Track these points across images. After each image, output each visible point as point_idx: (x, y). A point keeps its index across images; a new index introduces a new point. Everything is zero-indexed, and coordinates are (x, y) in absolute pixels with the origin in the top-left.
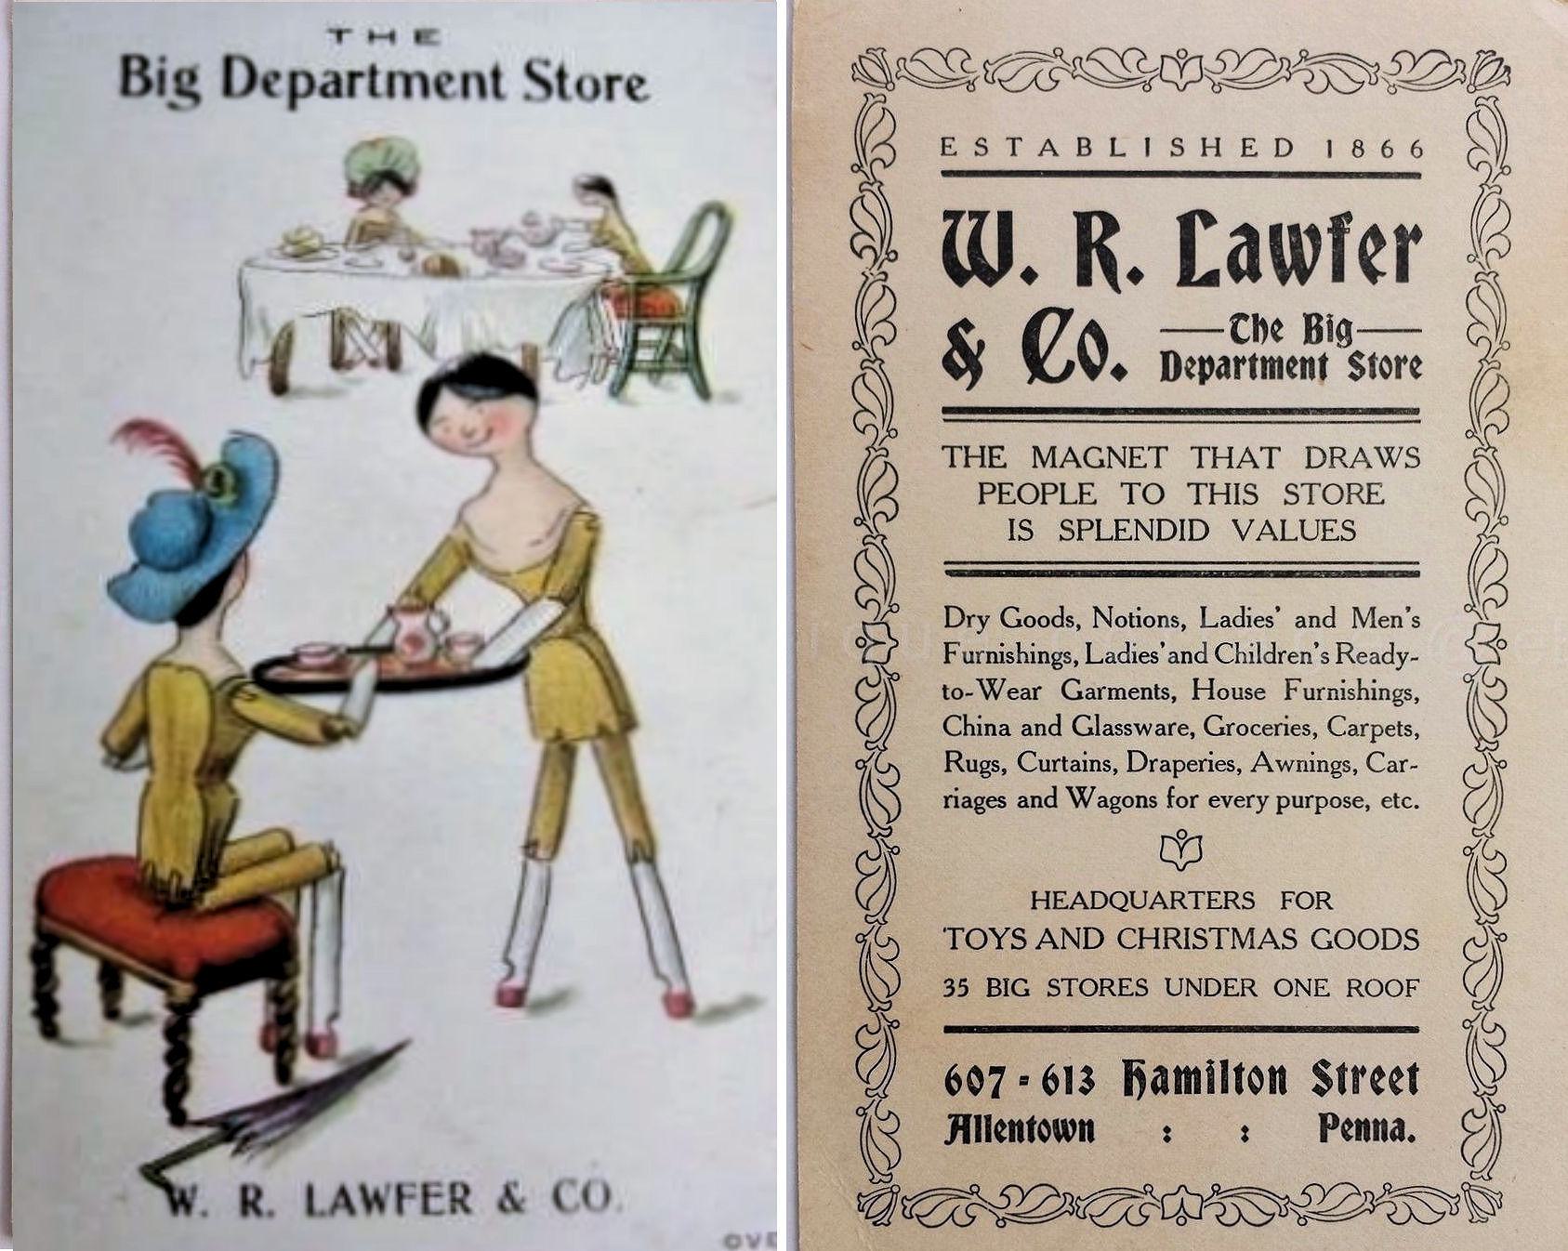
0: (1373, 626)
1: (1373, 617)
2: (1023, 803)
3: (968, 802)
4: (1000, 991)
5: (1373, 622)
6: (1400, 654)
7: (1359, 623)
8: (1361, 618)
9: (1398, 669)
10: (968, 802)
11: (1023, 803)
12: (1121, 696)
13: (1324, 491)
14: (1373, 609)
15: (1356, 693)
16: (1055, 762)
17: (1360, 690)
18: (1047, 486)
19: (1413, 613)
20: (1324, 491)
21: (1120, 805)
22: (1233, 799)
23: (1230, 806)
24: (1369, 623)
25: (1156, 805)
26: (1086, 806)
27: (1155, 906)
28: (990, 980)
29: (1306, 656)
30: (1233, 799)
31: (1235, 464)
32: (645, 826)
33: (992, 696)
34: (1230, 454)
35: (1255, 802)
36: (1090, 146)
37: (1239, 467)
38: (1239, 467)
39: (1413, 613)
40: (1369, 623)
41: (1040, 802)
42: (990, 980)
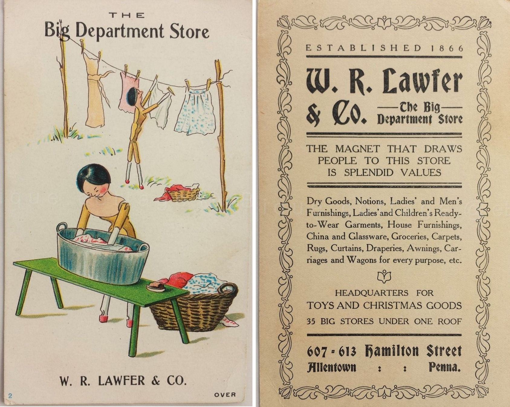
0: (447, 204)
1: (447, 201)
2: (333, 261)
5: (447, 202)
6: (455, 213)
9: (455, 218)
11: (333, 261)
12: (364, 226)
13: (431, 160)
14: (446, 198)
19: (460, 199)
20: (431, 160)
21: (364, 262)
22: (401, 260)
24: (445, 203)
25: (376, 262)
26: (353, 262)
30: (401, 260)
31: (402, 151)
34: (400, 148)
35: (408, 261)
37: (403, 152)
38: (403, 152)
39: (460, 199)
41: (338, 261)
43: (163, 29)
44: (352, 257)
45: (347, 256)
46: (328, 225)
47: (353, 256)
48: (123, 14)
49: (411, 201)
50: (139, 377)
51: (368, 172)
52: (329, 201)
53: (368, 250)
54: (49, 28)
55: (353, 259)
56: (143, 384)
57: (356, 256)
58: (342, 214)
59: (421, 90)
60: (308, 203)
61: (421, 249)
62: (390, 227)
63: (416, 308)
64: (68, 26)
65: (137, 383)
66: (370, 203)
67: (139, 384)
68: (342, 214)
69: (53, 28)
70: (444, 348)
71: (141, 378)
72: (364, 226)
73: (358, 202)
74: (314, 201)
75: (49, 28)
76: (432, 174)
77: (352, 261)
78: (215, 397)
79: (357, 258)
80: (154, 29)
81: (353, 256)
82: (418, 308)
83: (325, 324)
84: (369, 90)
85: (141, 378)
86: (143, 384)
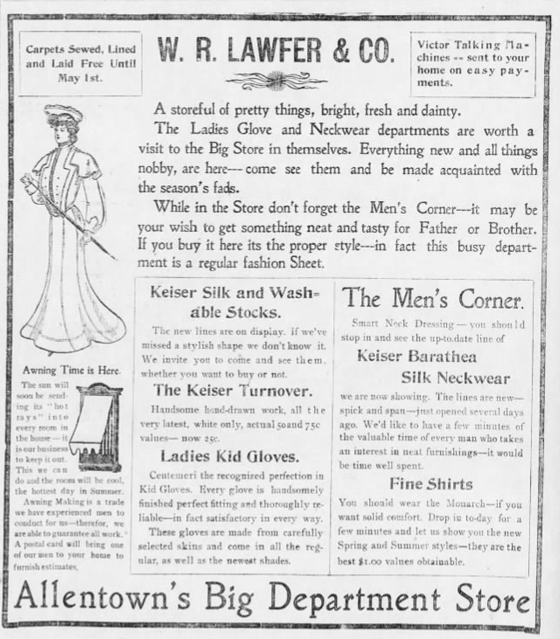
1: (410, 298)
3: (464, 453)
4: (224, 601)
7: (398, 303)
8: (400, 298)
10: (464, 453)
12: (385, 604)
15: (384, 111)
16: (406, 130)
17: (387, 109)
18: (213, 586)
19: (441, 294)
23: (167, 211)
27: (476, 147)
28: (211, 143)
29: (429, 300)
32: (360, 52)
33: (137, 606)
36: (210, 49)
39: (441, 294)
40: (406, 303)
42: (211, 143)
43: (439, 596)
49: (203, 454)
52: (469, 299)
53: (273, 603)
54: (215, 595)
59: (137, 606)
60: (193, 133)
61: (150, 599)
64: (252, 595)
66: (367, 606)
69: (223, 594)
70: (512, 599)
72: (385, 604)
73: (315, 130)
74: (446, 398)
75: (215, 595)
78: (66, 608)
80: (385, 595)
83: (222, 606)
84: (392, 60)
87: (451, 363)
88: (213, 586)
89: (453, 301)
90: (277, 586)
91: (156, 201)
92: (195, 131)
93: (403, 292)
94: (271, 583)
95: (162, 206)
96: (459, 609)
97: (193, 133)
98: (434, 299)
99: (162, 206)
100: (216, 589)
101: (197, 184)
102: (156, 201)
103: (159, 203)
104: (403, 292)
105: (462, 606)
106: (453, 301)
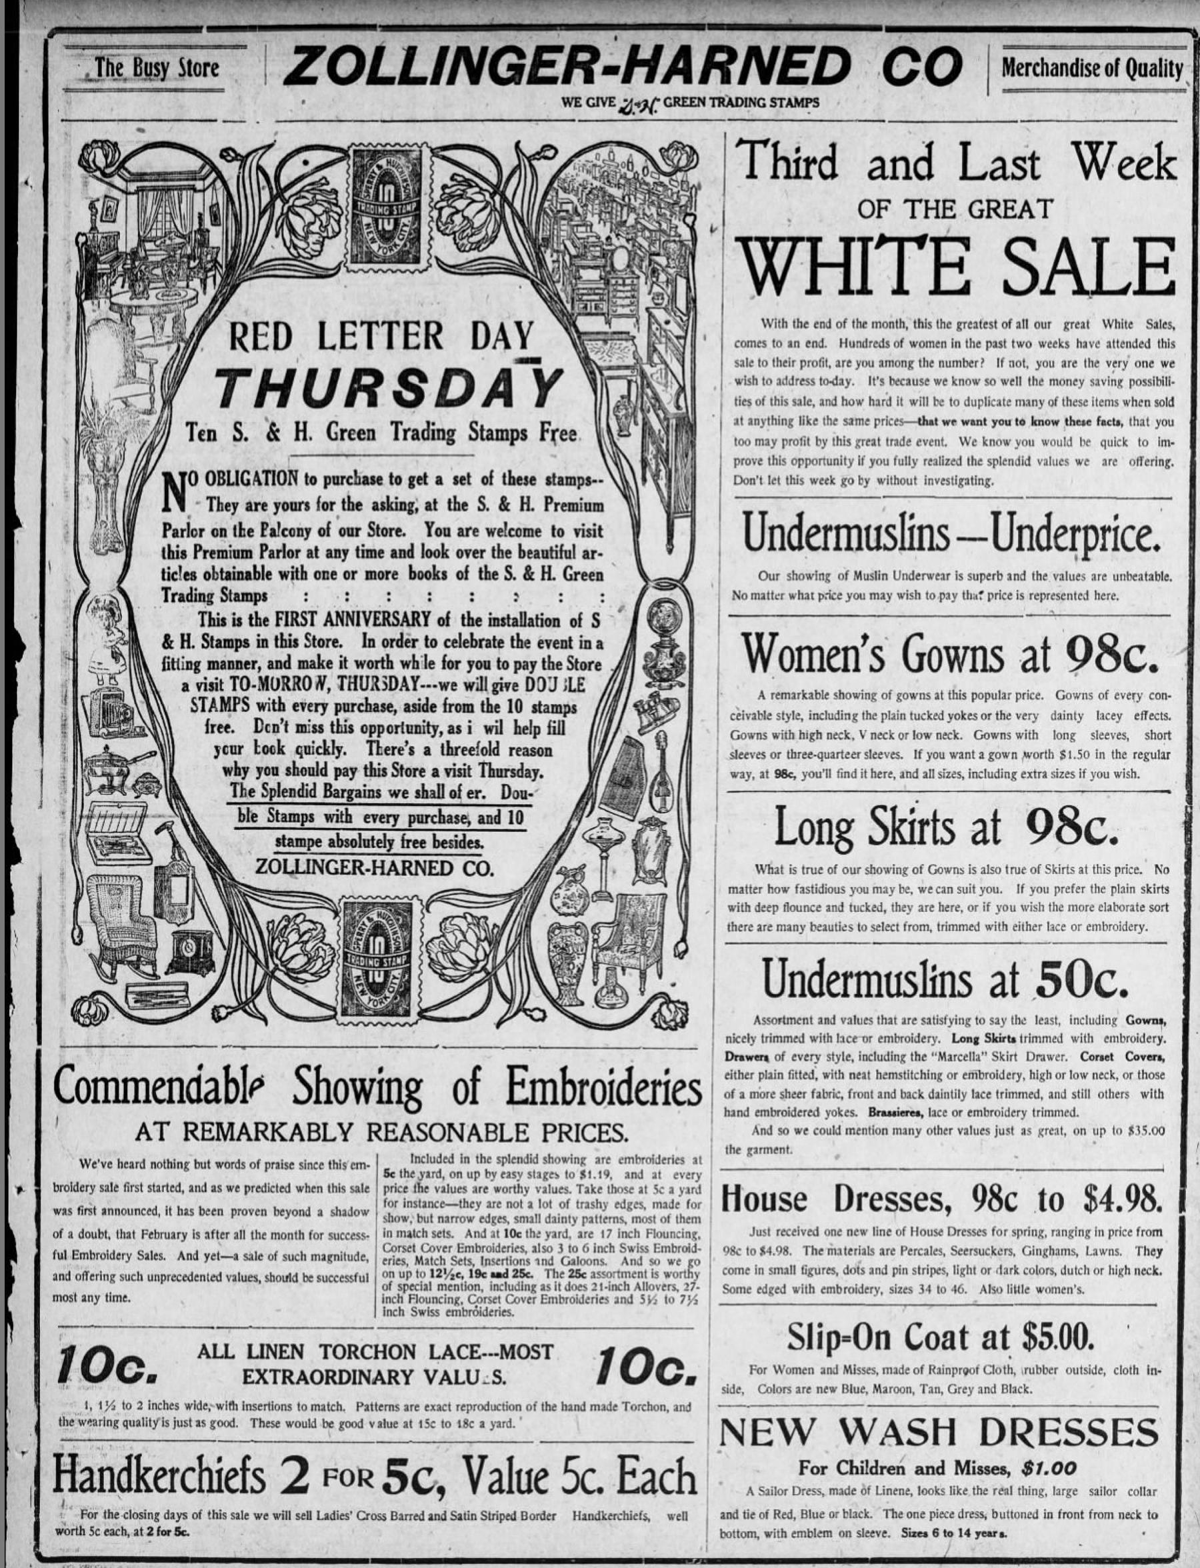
33: (769, 285)
44: (1094, 146)
45: (1175, 178)
46: (1121, 168)
47: (1099, 143)
48: (1107, 240)
50: (428, 324)
51: (289, 1350)
55: (1101, 157)
56: (439, 346)
57: (1112, 144)
58: (838, 828)
59: (769, 285)
60: (964, 177)
62: (819, 292)
63: (904, 1440)
65: (421, 339)
67: (427, 346)
68: (838, 828)
71: (433, 329)
76: (630, 1483)
77: (1094, 170)
79: (779, 644)
81: (1099, 143)
82: (910, 1442)
85: (433, 329)
86: (439, 346)
87: (778, 553)
88: (944, 246)
89: (892, 656)
90: (820, 260)
91: (1077, 144)
92: (970, 173)
93: (225, 1127)
94: (870, 292)
95: (1094, 160)
96: (1008, 289)
97: (964, 177)
98: (861, 650)
99: (1094, 160)
100: (491, 1128)
101: (858, 642)
102: (1077, 144)
103: (755, 247)
104: (225, 1127)
105: (1014, 286)
106: (892, 656)
